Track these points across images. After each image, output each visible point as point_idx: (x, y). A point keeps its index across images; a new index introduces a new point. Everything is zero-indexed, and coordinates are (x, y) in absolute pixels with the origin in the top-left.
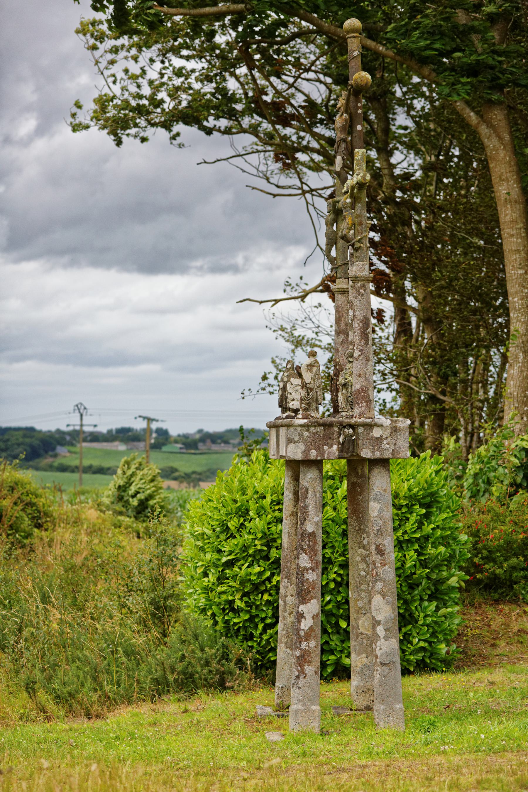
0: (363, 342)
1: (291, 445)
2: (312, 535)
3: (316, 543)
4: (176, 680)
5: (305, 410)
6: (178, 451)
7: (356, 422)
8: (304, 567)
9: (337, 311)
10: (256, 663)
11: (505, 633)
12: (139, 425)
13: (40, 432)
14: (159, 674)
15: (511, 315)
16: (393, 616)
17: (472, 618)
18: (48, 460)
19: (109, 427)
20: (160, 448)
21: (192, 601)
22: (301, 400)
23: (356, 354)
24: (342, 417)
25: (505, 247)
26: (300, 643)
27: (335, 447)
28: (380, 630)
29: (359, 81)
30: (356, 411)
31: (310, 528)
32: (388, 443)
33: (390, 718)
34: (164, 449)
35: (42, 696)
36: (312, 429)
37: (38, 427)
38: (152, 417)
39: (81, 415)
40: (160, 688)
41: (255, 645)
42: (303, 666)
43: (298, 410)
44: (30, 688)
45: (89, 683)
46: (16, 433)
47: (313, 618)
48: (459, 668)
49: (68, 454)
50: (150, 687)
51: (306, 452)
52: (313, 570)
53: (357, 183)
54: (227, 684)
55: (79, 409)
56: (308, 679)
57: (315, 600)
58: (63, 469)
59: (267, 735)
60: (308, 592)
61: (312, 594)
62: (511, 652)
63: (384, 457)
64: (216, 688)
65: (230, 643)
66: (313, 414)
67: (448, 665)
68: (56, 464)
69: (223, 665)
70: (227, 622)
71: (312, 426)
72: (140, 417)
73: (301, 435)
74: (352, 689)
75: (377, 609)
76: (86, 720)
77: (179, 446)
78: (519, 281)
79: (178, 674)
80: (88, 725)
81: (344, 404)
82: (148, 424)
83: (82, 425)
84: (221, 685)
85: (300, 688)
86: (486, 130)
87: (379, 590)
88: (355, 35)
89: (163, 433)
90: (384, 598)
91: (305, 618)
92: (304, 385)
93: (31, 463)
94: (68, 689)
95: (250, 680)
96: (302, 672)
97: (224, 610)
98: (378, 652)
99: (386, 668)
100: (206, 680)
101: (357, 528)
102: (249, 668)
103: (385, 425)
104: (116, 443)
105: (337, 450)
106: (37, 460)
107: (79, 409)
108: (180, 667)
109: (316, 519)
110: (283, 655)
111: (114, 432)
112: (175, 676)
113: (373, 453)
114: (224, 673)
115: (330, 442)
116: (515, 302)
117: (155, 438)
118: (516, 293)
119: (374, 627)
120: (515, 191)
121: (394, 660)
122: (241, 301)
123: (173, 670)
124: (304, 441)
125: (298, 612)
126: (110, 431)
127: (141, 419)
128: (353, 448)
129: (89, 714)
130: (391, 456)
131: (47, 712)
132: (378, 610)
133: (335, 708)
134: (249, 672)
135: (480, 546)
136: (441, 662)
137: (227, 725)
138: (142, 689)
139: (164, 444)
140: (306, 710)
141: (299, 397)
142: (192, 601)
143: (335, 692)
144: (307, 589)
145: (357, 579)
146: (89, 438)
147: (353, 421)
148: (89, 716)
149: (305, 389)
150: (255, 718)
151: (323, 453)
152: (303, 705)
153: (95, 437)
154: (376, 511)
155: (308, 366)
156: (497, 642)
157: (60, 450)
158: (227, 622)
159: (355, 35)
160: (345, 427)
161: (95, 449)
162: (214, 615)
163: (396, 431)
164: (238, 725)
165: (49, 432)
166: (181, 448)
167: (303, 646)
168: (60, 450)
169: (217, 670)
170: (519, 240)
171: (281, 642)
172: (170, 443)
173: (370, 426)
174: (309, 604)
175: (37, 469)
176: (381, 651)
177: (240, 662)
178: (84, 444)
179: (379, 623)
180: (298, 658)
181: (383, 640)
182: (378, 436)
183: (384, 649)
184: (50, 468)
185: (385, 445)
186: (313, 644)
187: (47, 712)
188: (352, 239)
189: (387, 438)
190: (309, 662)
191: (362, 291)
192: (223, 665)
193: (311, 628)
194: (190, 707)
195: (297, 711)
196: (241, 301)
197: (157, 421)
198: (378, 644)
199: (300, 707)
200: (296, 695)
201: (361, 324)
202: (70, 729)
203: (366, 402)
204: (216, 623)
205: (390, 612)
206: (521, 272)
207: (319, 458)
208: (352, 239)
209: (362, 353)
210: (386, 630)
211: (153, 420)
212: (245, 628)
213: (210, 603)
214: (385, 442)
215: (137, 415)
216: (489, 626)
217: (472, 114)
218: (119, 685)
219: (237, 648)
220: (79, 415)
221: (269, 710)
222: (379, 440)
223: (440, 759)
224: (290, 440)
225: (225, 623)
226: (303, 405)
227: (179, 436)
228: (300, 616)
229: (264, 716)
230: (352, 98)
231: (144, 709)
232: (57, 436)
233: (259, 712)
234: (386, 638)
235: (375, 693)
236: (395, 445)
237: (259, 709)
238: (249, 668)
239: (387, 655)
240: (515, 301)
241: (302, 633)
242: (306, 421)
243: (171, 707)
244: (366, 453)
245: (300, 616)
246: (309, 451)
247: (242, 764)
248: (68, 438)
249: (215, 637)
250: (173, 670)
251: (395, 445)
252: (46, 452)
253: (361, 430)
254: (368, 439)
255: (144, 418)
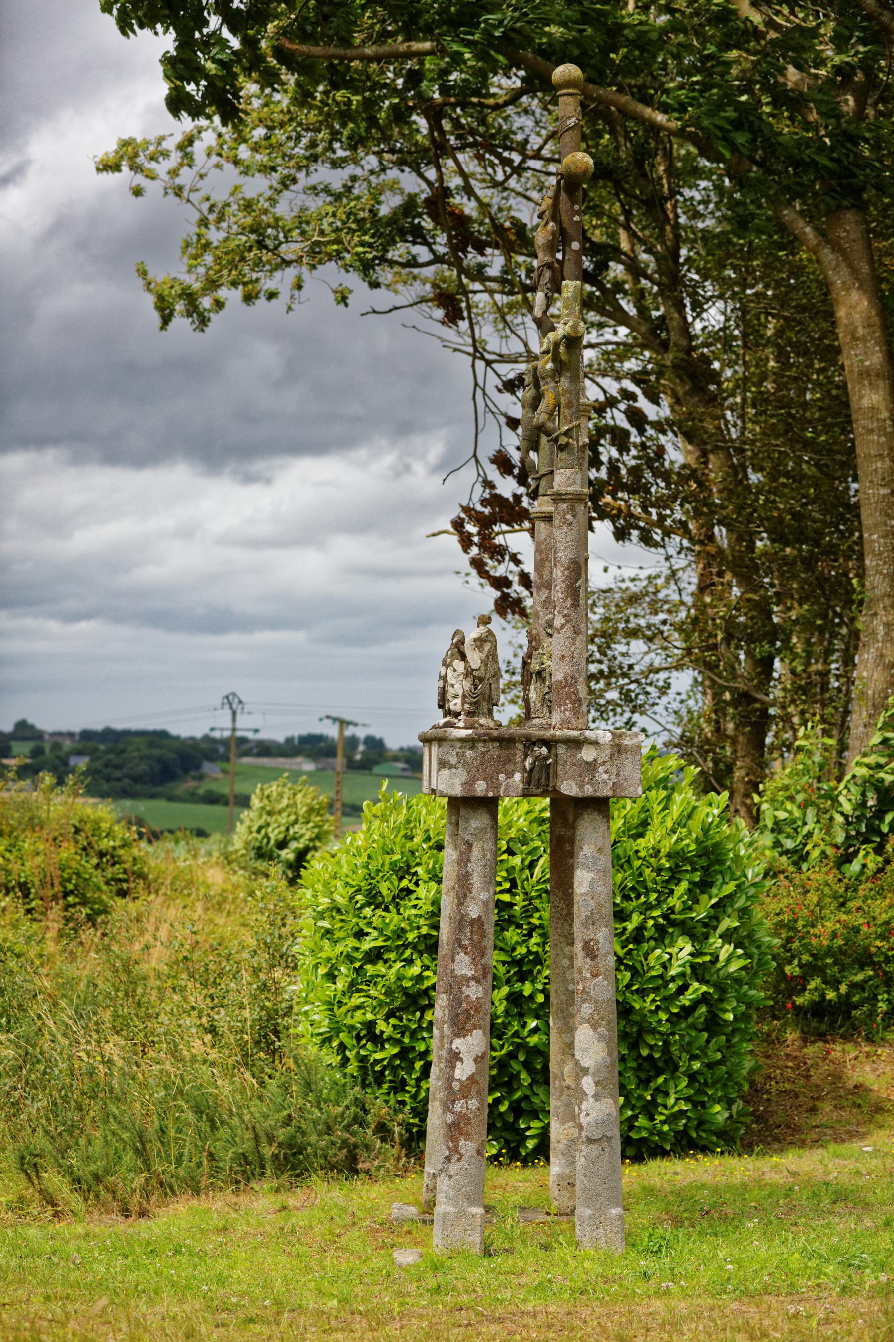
0: (569, 602)
1: (446, 772)
2: (479, 921)
3: (483, 936)
4: (275, 1157)
5: (470, 714)
6: (400, 773)
7: (554, 736)
8: (463, 976)
9: (538, 550)
10: (409, 1130)
11: (833, 1091)
12: (332, 731)
13: (177, 738)
14: (247, 1146)
15: (867, 562)
16: (609, 1060)
17: (780, 1063)
18: (187, 785)
19: (289, 734)
20: (370, 769)
21: (308, 1024)
22: (464, 696)
23: (557, 623)
24: (533, 729)
25: (859, 450)
26: (453, 1102)
27: (517, 777)
28: (588, 1084)
29: (572, 167)
30: (556, 718)
31: (474, 911)
32: (606, 772)
33: (601, 1230)
34: (377, 770)
35: (53, 1180)
36: (481, 747)
37: (174, 730)
38: (348, 718)
39: (234, 713)
40: (248, 1170)
41: (407, 1098)
42: (458, 1140)
43: (459, 714)
44: (30, 1166)
45: (128, 1157)
46: (138, 739)
47: (475, 1060)
48: (748, 1148)
49: (220, 776)
50: (231, 1168)
51: (469, 784)
52: (478, 981)
53: (564, 337)
54: (360, 1166)
55: (230, 704)
56: (464, 1162)
57: (480, 1032)
58: (213, 799)
59: (395, 1255)
60: (469, 1017)
61: (474, 1021)
62: (840, 1121)
63: (598, 794)
64: (340, 1171)
65: (368, 1095)
66: (482, 721)
67: (731, 1140)
68: (201, 791)
69: (354, 1134)
70: (363, 1059)
71: (479, 740)
72: (328, 717)
73: (460, 756)
74: (551, 1179)
75: (586, 1049)
76: (121, 1219)
77: (401, 765)
78: (881, 505)
79: (280, 1145)
80: (122, 1226)
81: (539, 705)
82: (341, 731)
83: (234, 729)
84: (349, 1165)
85: (451, 1177)
86: (831, 257)
87: (588, 1017)
88: (570, 91)
89: (375, 744)
90: (595, 1030)
91: (461, 1060)
92: (469, 673)
93: (160, 789)
94: (93, 1167)
95: (398, 1159)
96: (456, 1150)
97: (358, 1038)
98: (583, 1120)
99: (595, 1148)
100: (325, 1157)
101: (564, 912)
102: (397, 1139)
103: (602, 741)
104: (299, 760)
105: (522, 781)
106: (170, 785)
107: (230, 704)
108: (282, 1134)
109: (484, 896)
110: (436, 1121)
111: (296, 741)
112: (274, 1149)
113: (581, 787)
114: (355, 1146)
115: (509, 767)
116: (872, 541)
117: (363, 753)
118: (876, 525)
119: (578, 1078)
120: (875, 359)
121: (609, 1134)
122: (434, 535)
123: (271, 1139)
124: (466, 765)
125: (450, 1050)
126: (289, 740)
127: (330, 721)
128: (548, 779)
129: (127, 1210)
130: (610, 793)
131: (56, 1205)
132: (584, 1050)
133: (523, 1209)
134: (397, 1147)
135: (796, 945)
136: (715, 1134)
137: (339, 1236)
138: (218, 1169)
139: (376, 763)
140: (461, 1215)
141: (460, 693)
142: (308, 1024)
143: (516, 1181)
144: (467, 1012)
145: (563, 997)
146: (255, 750)
147: (548, 734)
148: (126, 1212)
149: (470, 679)
150: (388, 1225)
151: (498, 787)
152: (455, 1206)
153: (266, 749)
154: (586, 884)
155: (475, 640)
156: (819, 1104)
157: (207, 767)
158: (363, 1059)
159: (570, 91)
160: (534, 743)
161: (264, 768)
162: (342, 1047)
163: (619, 751)
164: (353, 1239)
165: (192, 738)
166: (404, 770)
167: (458, 1107)
168: (207, 767)
169: (345, 1142)
170: (883, 439)
171: (435, 1099)
172: (386, 760)
173: (576, 744)
174: (469, 1038)
175: (171, 799)
176: (589, 1119)
177: (383, 1130)
178: (246, 760)
179: (585, 1071)
180: (449, 1127)
181: (591, 1100)
182: (590, 759)
183: (593, 1115)
184: (193, 798)
185: (601, 775)
186: (474, 1104)
187: (56, 1205)
188: (555, 430)
189: (604, 763)
190: (468, 1134)
191: (569, 517)
192: (354, 1134)
193: (471, 1078)
194: (291, 1202)
195: (445, 1215)
196: (434, 535)
197: (356, 725)
198: (583, 1107)
199: (451, 1209)
200: (445, 1189)
201: (566, 573)
202: (87, 1234)
203: (573, 703)
204: (345, 1061)
205: (605, 1054)
206: (885, 491)
207: (490, 794)
208: (555, 430)
209: (568, 621)
210: (597, 1084)
211: (349, 723)
212: (394, 1069)
213: (336, 1029)
214: (601, 770)
215: (323, 715)
216: (807, 1077)
217: (808, 229)
218: (179, 1160)
219: (380, 1104)
220: (230, 712)
221: (413, 1210)
222: (592, 766)
223: (658, 1304)
224: (442, 764)
225: (361, 1061)
226: (466, 706)
227: (402, 749)
228: (455, 1057)
229: (401, 1221)
230: (563, 196)
231: (216, 1206)
232: (204, 746)
233: (395, 1213)
234: (597, 1097)
235: (577, 1188)
236: (618, 775)
237: (396, 1209)
238: (397, 1139)
239: (598, 1124)
240: (874, 540)
241: (456, 1085)
242: (470, 731)
243: (262, 1201)
244: (569, 788)
245: (455, 1057)
246: (474, 782)
247: (330, 1305)
248: (221, 749)
249: (344, 1085)
250: (271, 1139)
251: (618, 775)
252: (186, 771)
253: (561, 750)
254: (573, 765)
255: (335, 719)
